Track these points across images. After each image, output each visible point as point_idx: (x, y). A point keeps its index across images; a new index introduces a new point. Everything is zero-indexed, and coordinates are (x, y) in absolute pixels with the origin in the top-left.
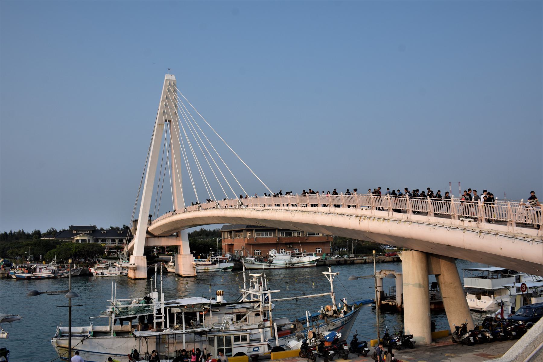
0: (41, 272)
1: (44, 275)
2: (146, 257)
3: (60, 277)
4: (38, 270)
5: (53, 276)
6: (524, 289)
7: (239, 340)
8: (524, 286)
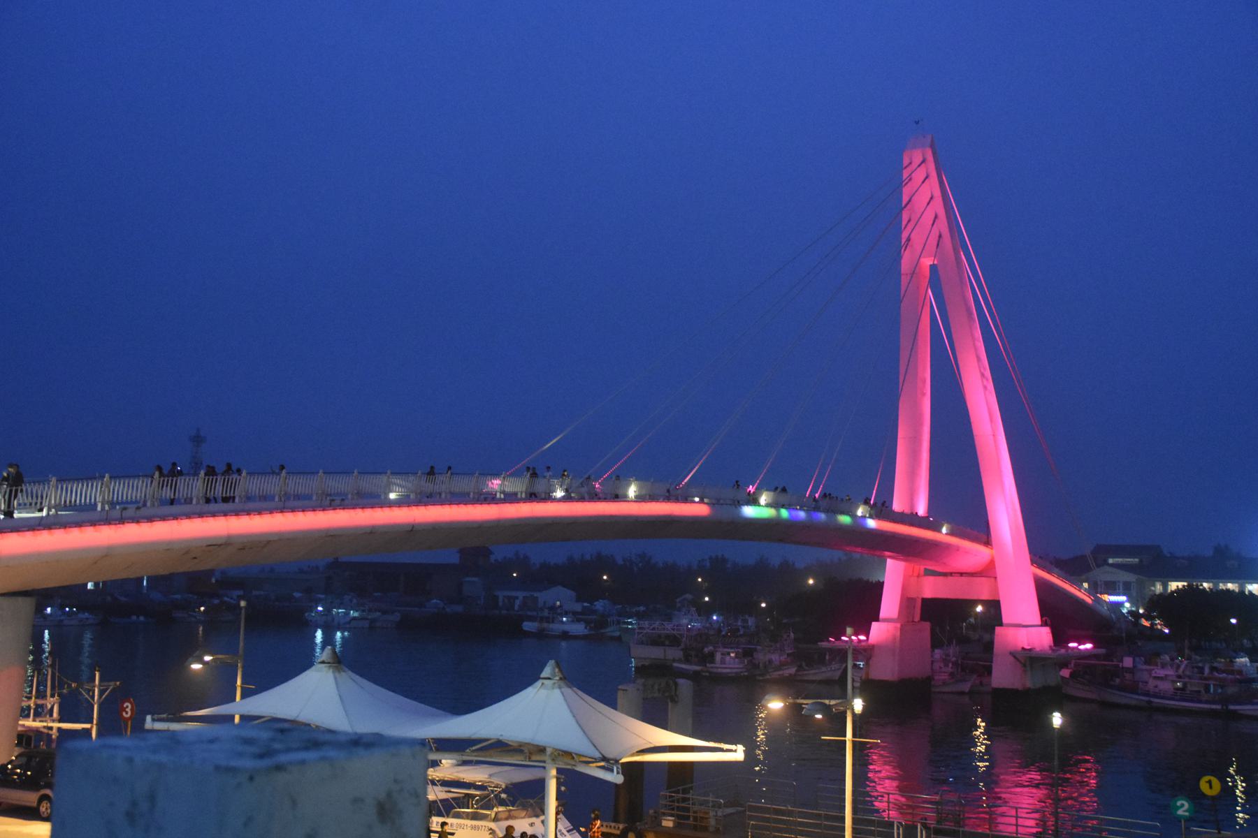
0: (725, 664)
1: (728, 670)
2: (927, 625)
3: (761, 678)
4: (718, 657)
5: (746, 674)
6: (127, 713)
7: (28, 716)
8: (127, 707)
